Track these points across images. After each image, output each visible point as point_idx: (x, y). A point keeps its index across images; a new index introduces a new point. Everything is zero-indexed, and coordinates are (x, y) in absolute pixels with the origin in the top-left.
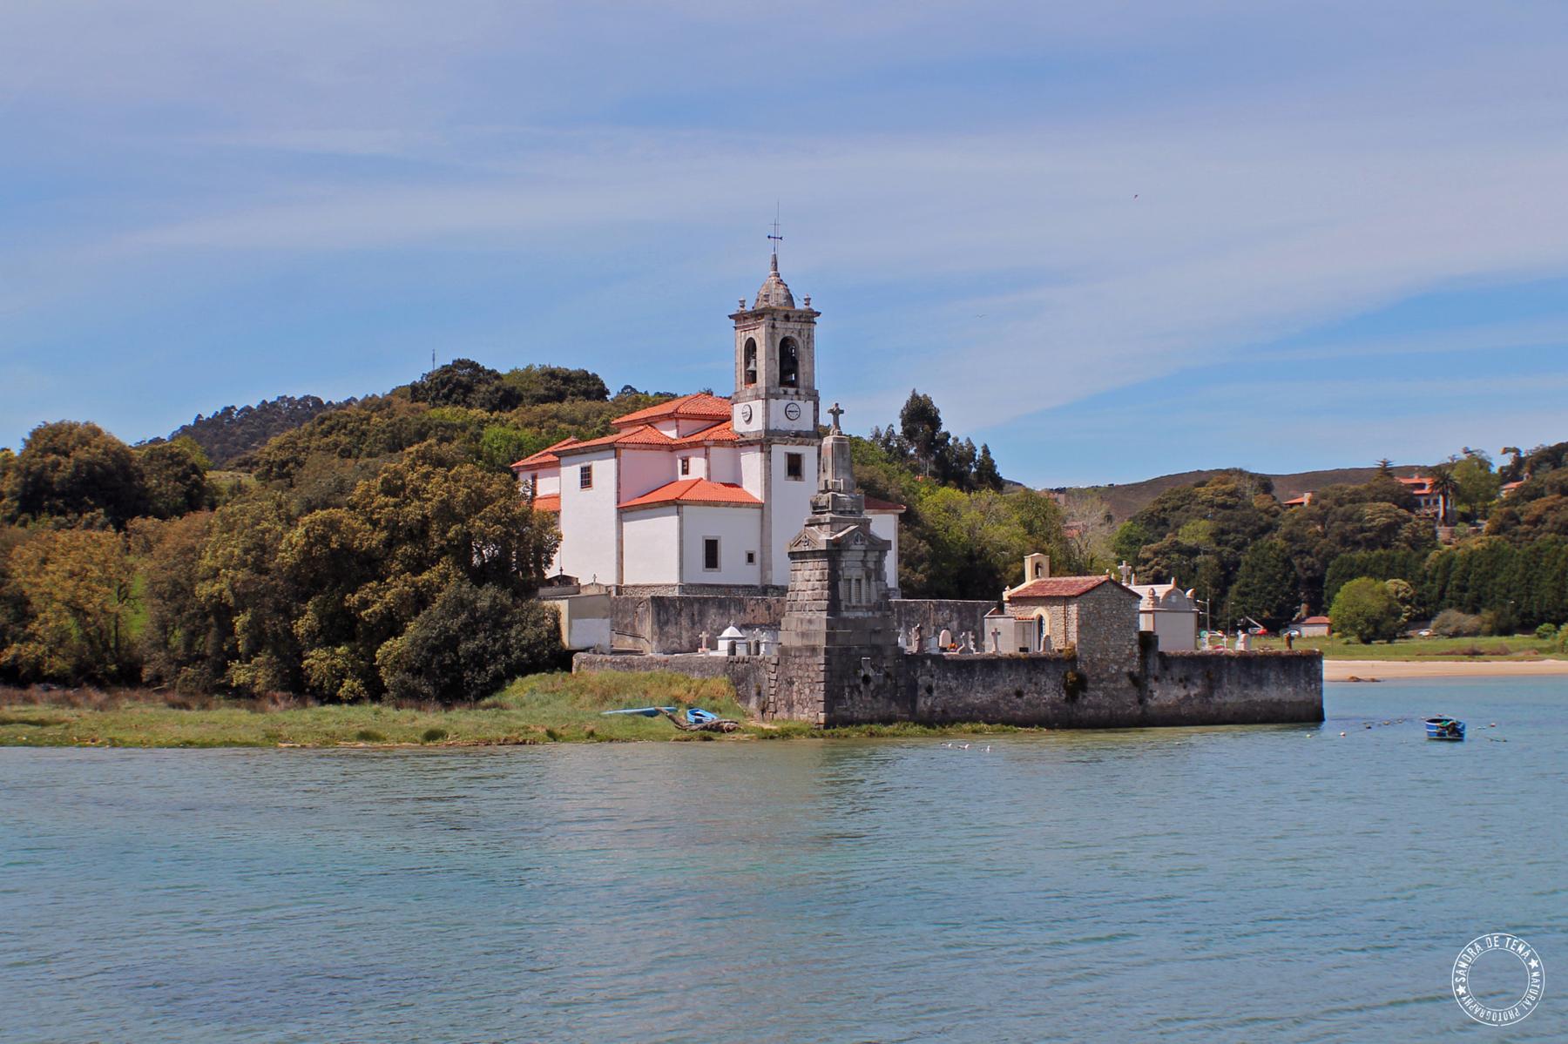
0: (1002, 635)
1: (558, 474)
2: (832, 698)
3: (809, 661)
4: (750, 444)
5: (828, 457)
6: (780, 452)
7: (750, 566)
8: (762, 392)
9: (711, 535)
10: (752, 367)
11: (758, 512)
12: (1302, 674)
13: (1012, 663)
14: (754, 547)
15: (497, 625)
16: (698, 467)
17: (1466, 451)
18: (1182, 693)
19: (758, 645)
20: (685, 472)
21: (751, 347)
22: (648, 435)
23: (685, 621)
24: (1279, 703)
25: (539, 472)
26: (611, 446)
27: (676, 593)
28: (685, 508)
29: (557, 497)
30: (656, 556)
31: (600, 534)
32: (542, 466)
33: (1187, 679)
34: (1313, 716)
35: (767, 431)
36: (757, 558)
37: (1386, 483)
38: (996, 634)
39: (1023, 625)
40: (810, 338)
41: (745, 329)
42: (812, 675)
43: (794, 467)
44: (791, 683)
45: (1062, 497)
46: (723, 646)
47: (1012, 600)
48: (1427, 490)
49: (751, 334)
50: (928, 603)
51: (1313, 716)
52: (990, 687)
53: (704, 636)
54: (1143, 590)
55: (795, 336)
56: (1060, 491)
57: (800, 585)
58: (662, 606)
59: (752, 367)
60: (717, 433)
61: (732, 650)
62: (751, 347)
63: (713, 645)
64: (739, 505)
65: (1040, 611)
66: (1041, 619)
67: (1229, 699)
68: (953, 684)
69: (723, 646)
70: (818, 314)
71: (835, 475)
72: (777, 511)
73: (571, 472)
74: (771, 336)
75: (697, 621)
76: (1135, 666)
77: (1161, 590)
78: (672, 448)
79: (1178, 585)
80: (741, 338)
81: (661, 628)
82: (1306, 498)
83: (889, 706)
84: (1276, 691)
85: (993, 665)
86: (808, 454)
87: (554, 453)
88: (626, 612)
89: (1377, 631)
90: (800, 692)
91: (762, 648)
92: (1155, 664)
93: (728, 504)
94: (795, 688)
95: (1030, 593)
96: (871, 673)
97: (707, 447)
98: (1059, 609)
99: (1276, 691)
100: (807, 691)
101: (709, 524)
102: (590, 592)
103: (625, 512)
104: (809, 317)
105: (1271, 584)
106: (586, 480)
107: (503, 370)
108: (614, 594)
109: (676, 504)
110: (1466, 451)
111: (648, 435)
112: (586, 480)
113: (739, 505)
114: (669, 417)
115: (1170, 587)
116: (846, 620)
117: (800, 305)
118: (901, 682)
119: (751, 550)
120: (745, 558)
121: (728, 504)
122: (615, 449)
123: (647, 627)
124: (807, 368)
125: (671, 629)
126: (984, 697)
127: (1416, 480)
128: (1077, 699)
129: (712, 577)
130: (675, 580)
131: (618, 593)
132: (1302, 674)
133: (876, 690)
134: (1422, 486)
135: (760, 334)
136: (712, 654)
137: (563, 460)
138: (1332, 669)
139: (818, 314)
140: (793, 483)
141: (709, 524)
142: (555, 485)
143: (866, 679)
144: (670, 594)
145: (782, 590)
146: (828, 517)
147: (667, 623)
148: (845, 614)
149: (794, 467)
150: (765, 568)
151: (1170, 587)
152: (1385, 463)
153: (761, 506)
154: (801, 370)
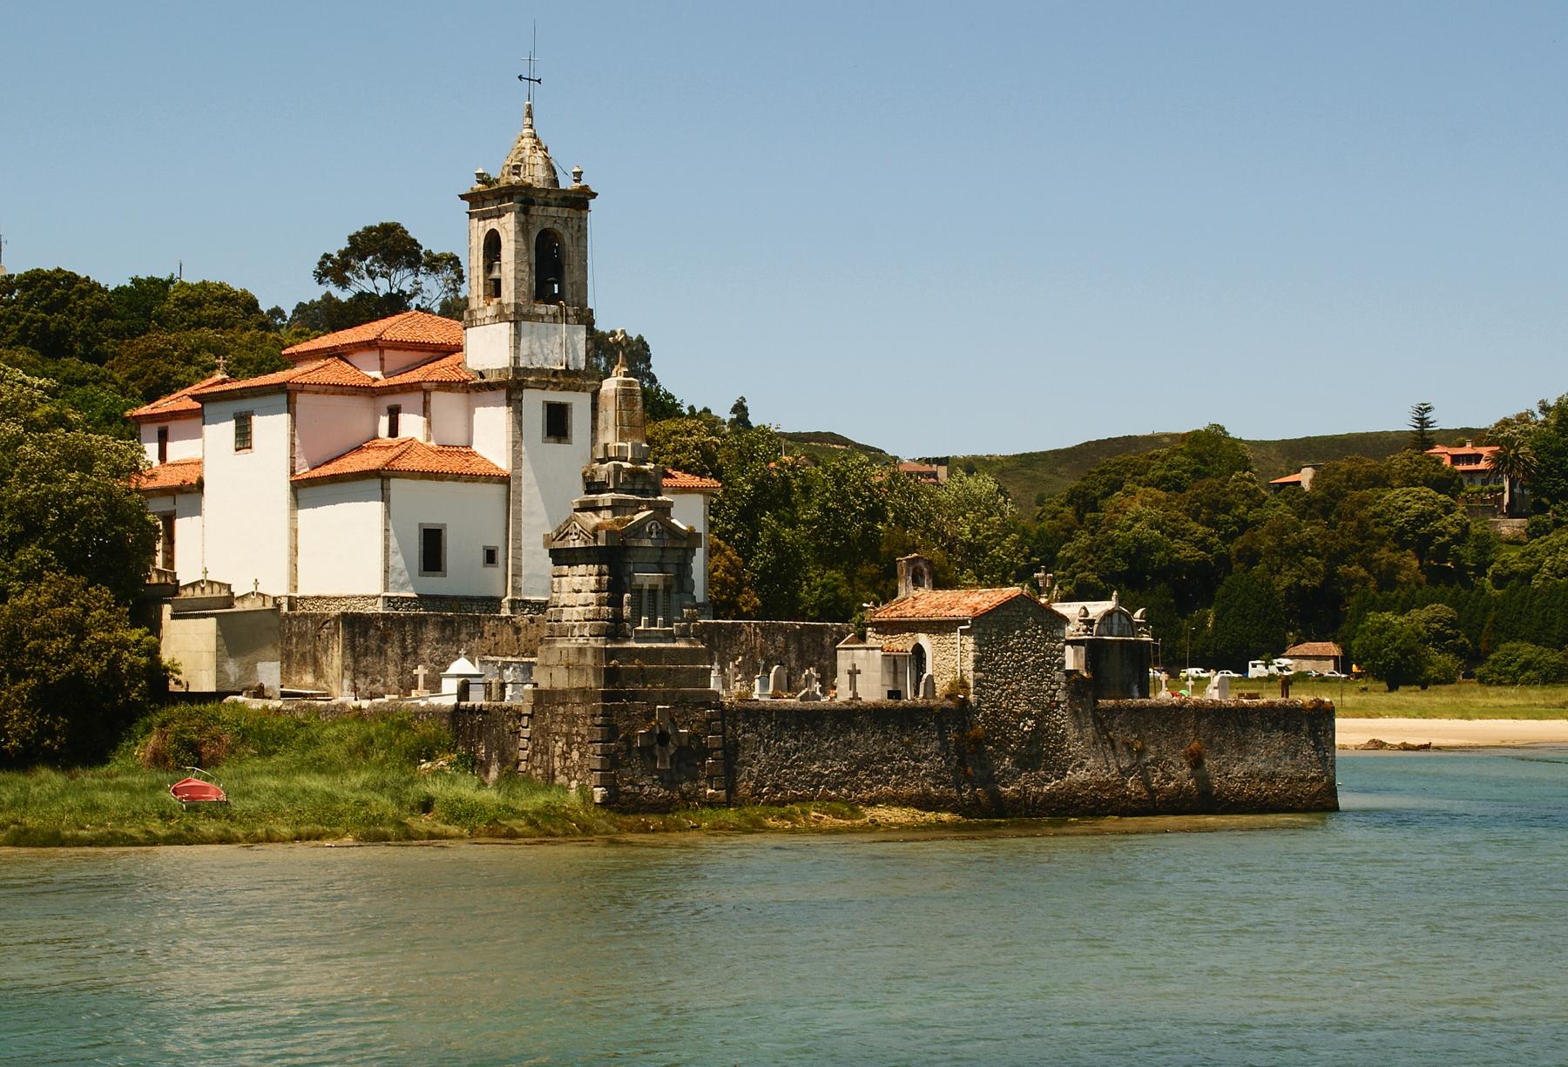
0: (862, 673)
1: (199, 435)
2: (612, 766)
4: (491, 387)
5: (609, 414)
6: (534, 401)
8: (509, 311)
9: (433, 520)
10: (495, 274)
11: (497, 490)
13: (875, 716)
14: (496, 541)
15: (1445, 637)
16: (412, 425)
19: (503, 686)
20: (393, 432)
21: (492, 244)
22: (335, 372)
23: (393, 651)
25: (173, 426)
26: (281, 388)
27: (380, 608)
28: (395, 483)
29: (199, 463)
30: (349, 556)
31: (254, 522)
32: (175, 415)
34: (1323, 802)
35: (517, 370)
36: (500, 556)
38: (853, 673)
39: (893, 663)
40: (582, 231)
41: (484, 217)
42: (583, 731)
43: (557, 424)
45: (942, 471)
46: (450, 686)
48: (1483, 465)
50: (748, 624)
51: (1323, 802)
53: (421, 671)
54: (1071, 610)
55: (558, 227)
56: (940, 461)
57: (565, 598)
58: (356, 625)
59: (495, 274)
60: (440, 370)
61: (464, 692)
62: (492, 244)
63: (434, 685)
64: (473, 478)
65: (923, 639)
66: (919, 651)
69: (450, 686)
70: (594, 195)
71: (622, 436)
72: (525, 485)
73: (221, 433)
74: (523, 229)
75: (409, 655)
77: (1097, 609)
78: (370, 392)
79: (1120, 601)
80: (480, 229)
81: (356, 661)
82: (1305, 476)
84: (1260, 761)
85: (853, 717)
86: (579, 403)
87: (194, 398)
88: (302, 635)
89: (1399, 671)
91: (509, 691)
93: (457, 477)
97: (426, 392)
99: (1260, 761)
100: (575, 755)
101: (427, 504)
102: (247, 606)
103: (305, 490)
104: (580, 200)
105: (1233, 601)
106: (244, 438)
108: (285, 609)
109: (380, 480)
111: (335, 372)
112: (244, 438)
113: (473, 478)
114: (369, 345)
115: (1109, 605)
117: (566, 183)
119: (491, 543)
120: (480, 556)
121: (457, 477)
122: (287, 395)
123: (335, 658)
124: (576, 275)
127: (1468, 449)
128: (977, 774)
129: (436, 585)
130: (376, 588)
131: (291, 607)
133: (668, 757)
134: (1477, 458)
135: (507, 226)
136: (435, 701)
137: (208, 409)
138: (1350, 732)
139: (594, 195)
141: (427, 504)
142: (207, 448)
144: (370, 610)
145: (542, 607)
146: (606, 498)
149: (557, 424)
151: (1109, 605)
153: (505, 480)
154: (568, 279)
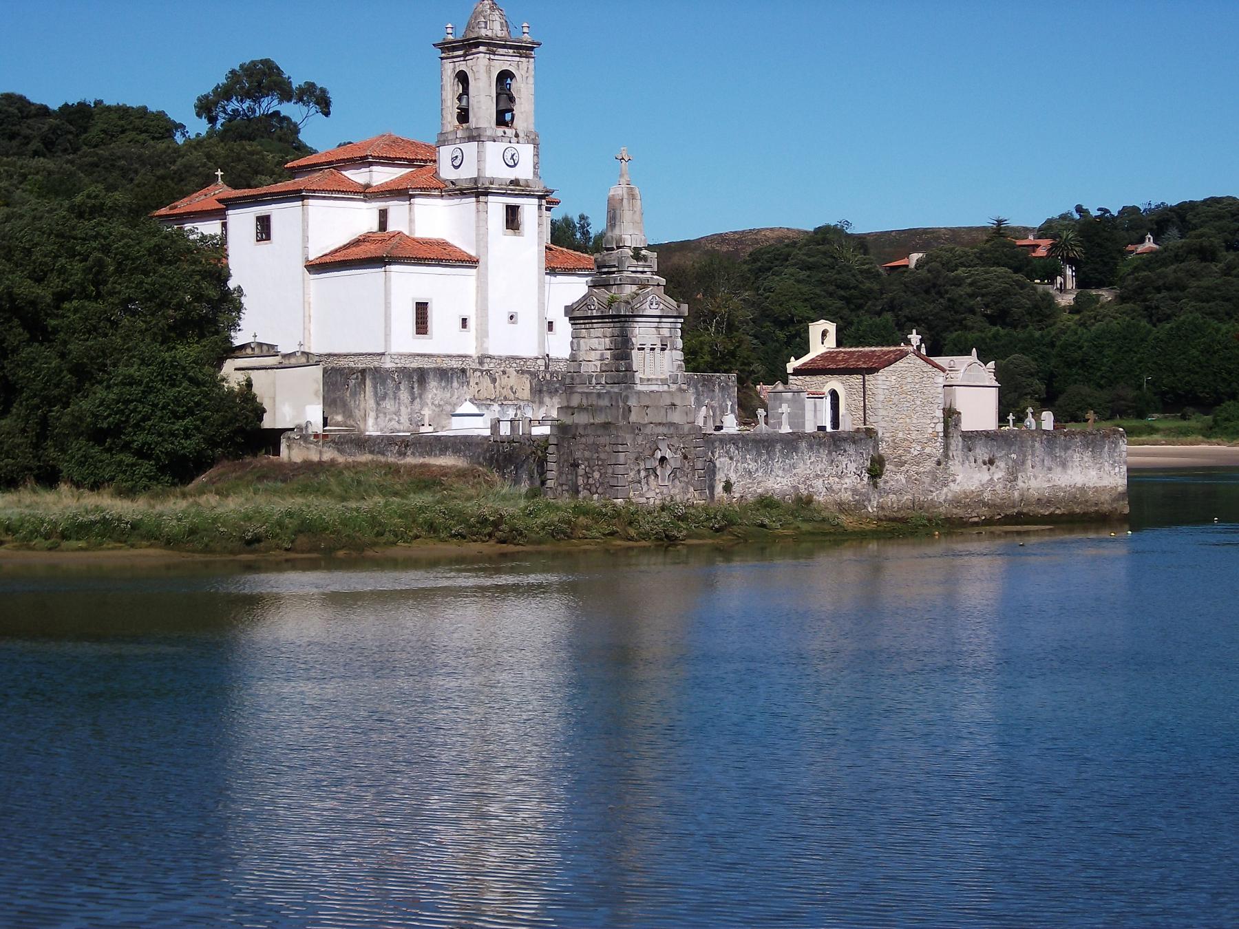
3: (602, 440)
7: (464, 333)
12: (1106, 456)
17: (1079, 209)
18: (985, 477)
24: (1083, 489)
33: (991, 462)
36: (472, 323)
37: (998, 243)
44: (575, 465)
47: (797, 372)
49: (462, 66)
52: (789, 471)
59: (464, 103)
66: (834, 395)
67: (1033, 484)
68: (752, 466)
73: (242, 221)
76: (936, 449)
80: (449, 69)
83: (686, 492)
90: (587, 476)
92: (956, 442)
94: (581, 471)
95: (820, 364)
96: (668, 454)
98: (856, 380)
100: (597, 475)
107: (54, 106)
110: (582, 217)
116: (639, 392)
118: (699, 465)
125: (388, 405)
126: (784, 481)
132: (1106, 456)
140: (510, 238)
143: (663, 460)
147: (384, 398)
148: (639, 387)
150: (483, 334)
152: (1000, 222)
